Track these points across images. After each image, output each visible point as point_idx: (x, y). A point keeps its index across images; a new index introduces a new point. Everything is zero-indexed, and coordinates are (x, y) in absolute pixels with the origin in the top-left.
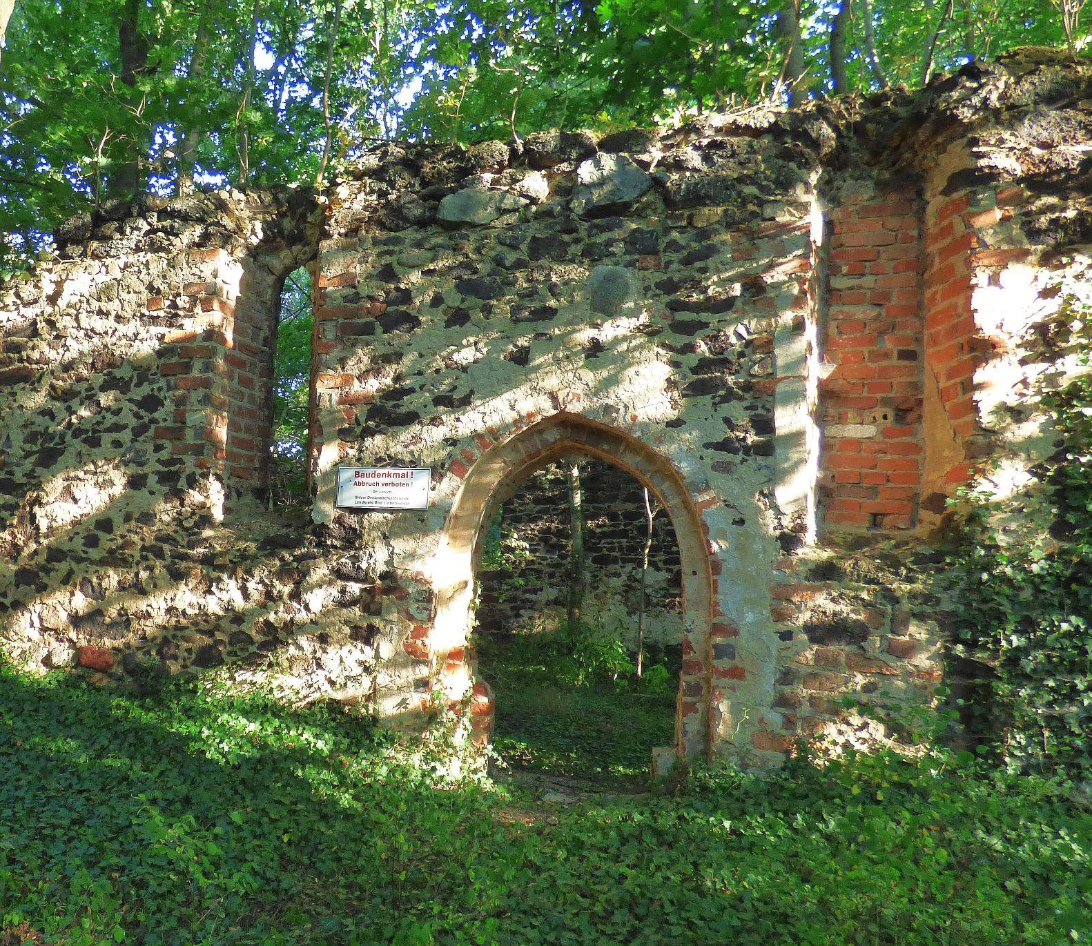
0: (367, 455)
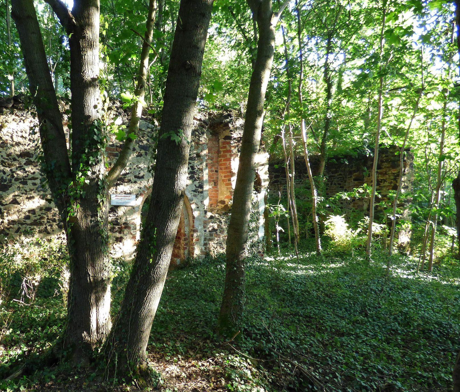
0: (118, 191)
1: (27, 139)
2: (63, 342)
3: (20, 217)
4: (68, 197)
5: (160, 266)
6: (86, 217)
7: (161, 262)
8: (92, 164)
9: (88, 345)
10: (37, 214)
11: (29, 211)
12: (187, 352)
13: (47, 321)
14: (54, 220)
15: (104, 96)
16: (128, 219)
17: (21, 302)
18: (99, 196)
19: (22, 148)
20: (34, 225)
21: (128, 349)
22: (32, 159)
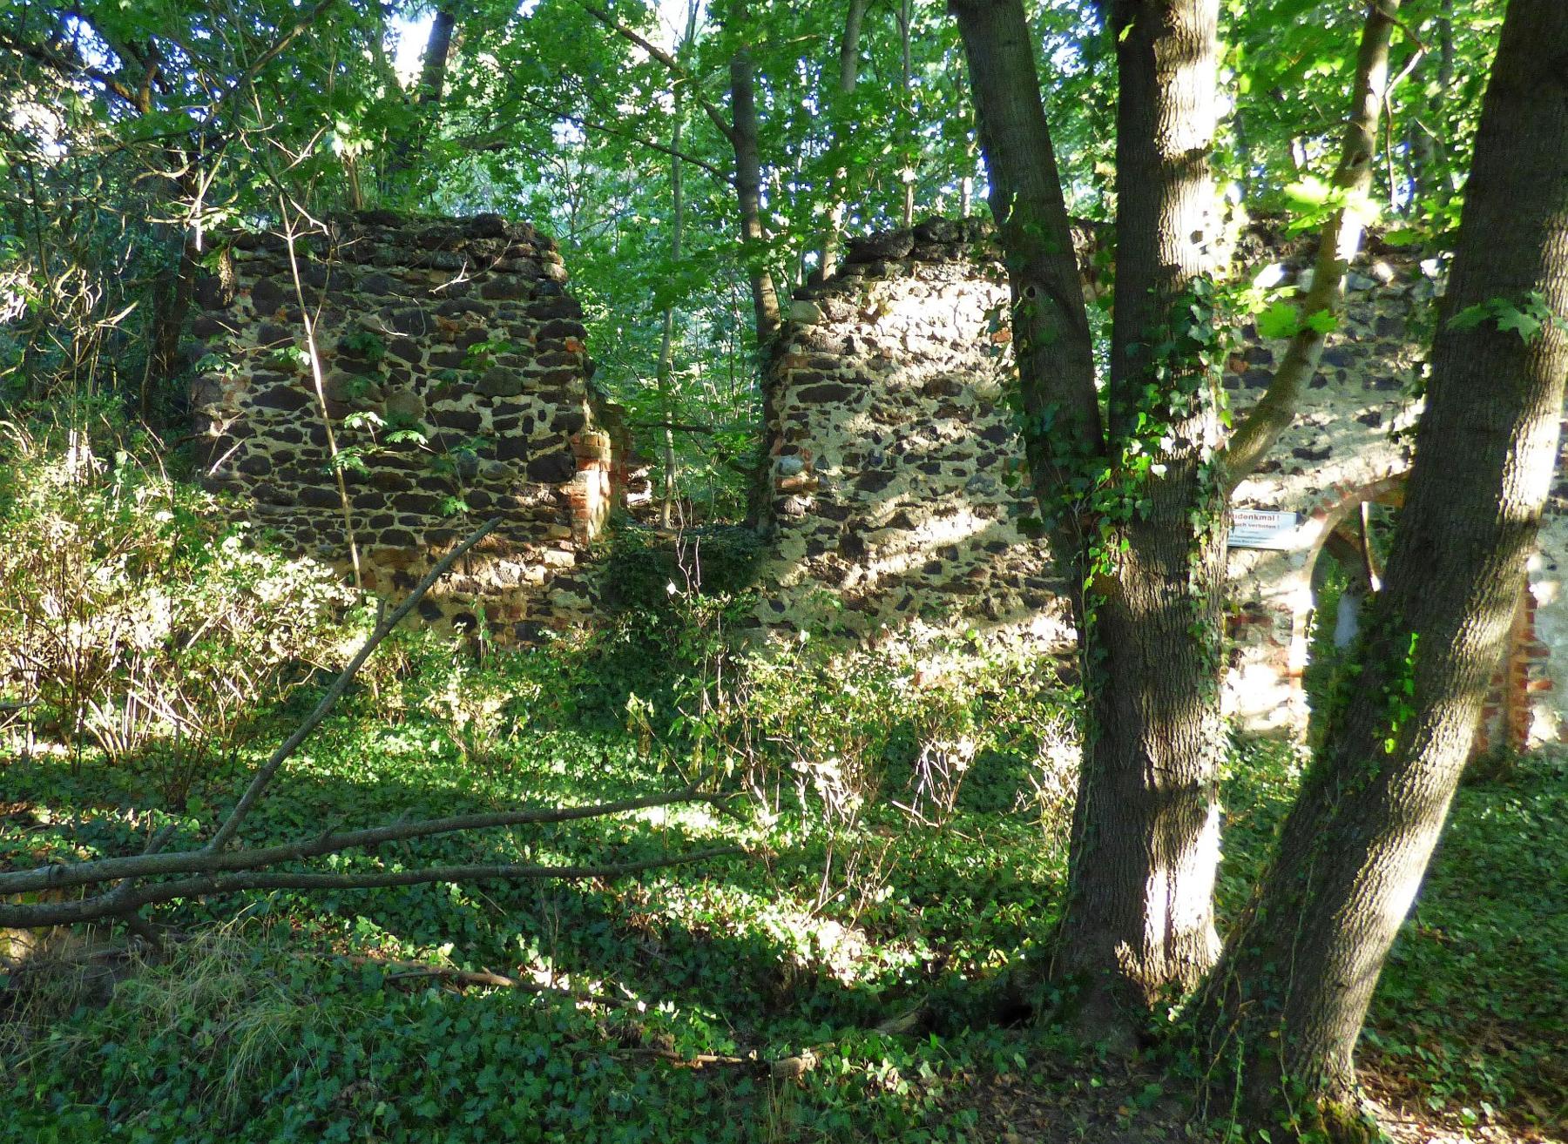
2: (1047, 960)
3: (913, 566)
4: (1092, 516)
5: (1427, 768)
6: (1149, 581)
7: (1429, 754)
8: (1178, 415)
9: (1133, 990)
10: (962, 559)
11: (940, 551)
12: (1517, 1100)
13: (990, 883)
14: (1013, 582)
15: (1228, 201)
18: (1195, 517)
19: (929, 369)
20: (952, 591)
21: (1286, 1033)
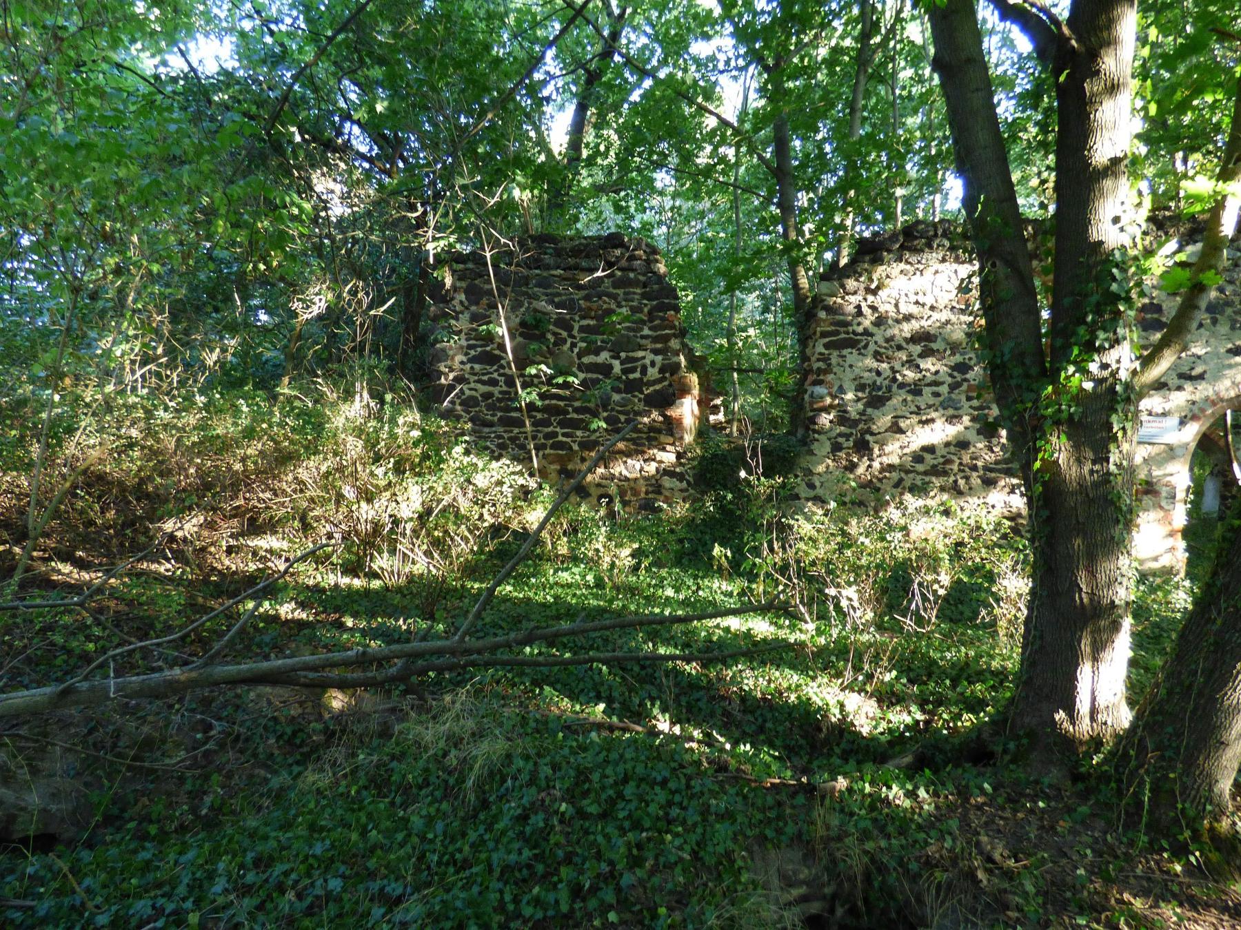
1: (927, 307)
2: (1006, 720)
6: (1079, 461)
9: (1069, 742)
13: (962, 669)
14: (974, 468)
16: (1155, 474)
17: (908, 622)
19: (915, 325)
21: (1181, 776)
22: (934, 346)
